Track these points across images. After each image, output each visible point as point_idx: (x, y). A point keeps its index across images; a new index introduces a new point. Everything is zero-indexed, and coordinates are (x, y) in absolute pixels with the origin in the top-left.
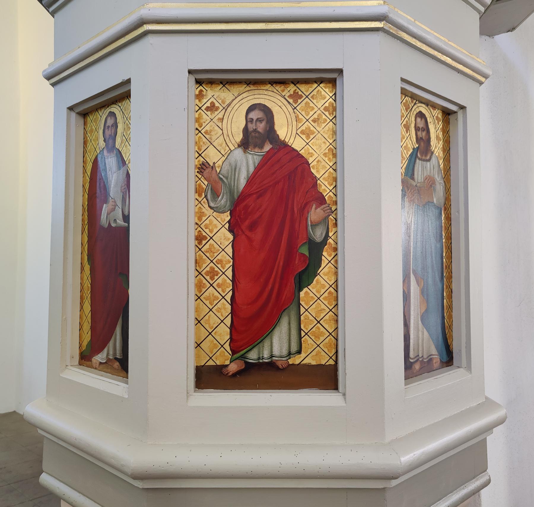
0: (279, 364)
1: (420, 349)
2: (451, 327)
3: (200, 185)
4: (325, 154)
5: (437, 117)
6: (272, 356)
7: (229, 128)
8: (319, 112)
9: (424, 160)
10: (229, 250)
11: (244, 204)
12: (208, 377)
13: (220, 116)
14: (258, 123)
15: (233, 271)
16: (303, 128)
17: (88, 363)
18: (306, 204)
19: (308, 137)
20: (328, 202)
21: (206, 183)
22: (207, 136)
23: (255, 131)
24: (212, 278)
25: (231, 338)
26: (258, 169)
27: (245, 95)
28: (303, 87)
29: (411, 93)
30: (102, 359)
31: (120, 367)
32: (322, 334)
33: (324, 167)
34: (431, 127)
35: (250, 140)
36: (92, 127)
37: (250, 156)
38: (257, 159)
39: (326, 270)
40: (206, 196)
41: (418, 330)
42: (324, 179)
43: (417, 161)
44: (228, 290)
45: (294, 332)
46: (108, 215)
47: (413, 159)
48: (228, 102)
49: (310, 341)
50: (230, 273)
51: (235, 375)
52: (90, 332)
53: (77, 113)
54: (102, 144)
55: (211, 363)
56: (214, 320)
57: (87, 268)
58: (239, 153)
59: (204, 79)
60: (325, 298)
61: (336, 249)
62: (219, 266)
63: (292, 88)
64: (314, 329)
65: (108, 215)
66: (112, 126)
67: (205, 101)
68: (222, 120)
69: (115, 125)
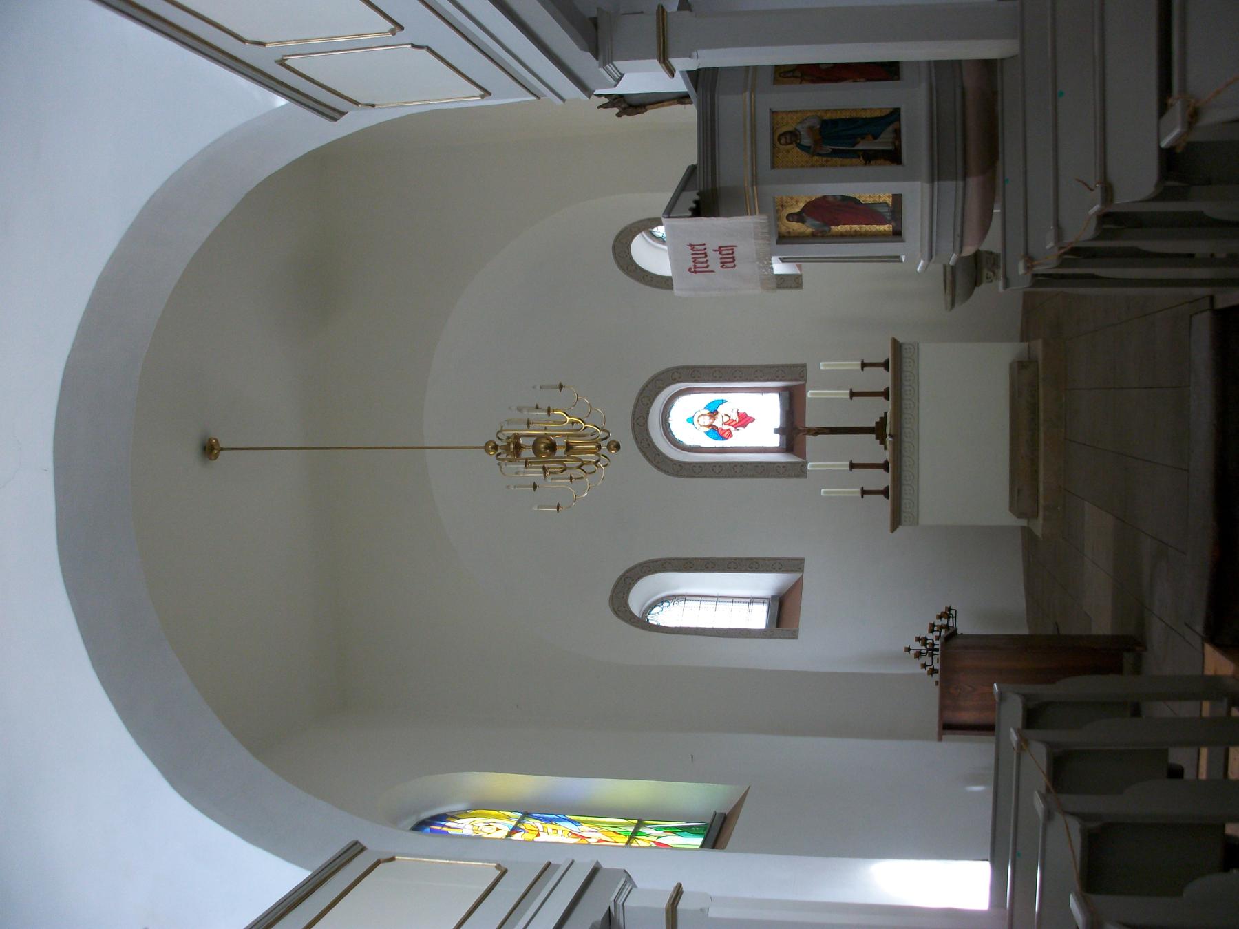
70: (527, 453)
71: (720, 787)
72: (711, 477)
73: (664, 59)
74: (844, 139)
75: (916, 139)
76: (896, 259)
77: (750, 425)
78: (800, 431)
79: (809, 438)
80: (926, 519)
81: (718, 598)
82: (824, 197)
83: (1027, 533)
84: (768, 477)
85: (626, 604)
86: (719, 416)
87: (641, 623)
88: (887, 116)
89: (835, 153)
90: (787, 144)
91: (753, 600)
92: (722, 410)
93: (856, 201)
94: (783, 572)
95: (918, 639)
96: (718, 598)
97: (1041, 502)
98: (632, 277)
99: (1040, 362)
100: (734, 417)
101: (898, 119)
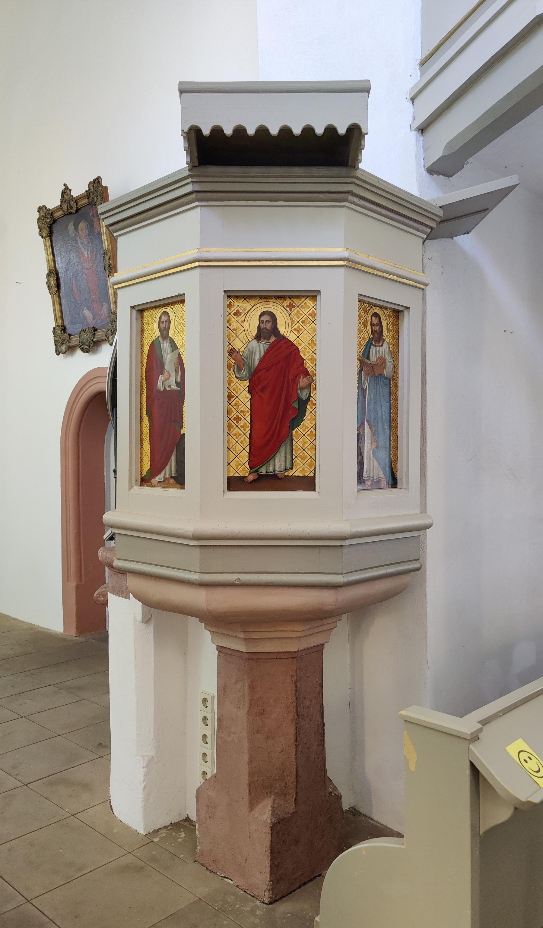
0: (279, 476)
1: (371, 472)
2: (396, 461)
3: (229, 363)
4: (309, 344)
5: (389, 315)
6: (275, 471)
7: (248, 327)
8: (306, 316)
9: (377, 346)
10: (248, 404)
11: (258, 375)
12: (234, 484)
13: (243, 319)
14: (267, 324)
15: (251, 418)
16: (295, 327)
17: (148, 484)
18: (297, 376)
19: (298, 333)
20: (311, 374)
21: (234, 362)
22: (234, 332)
23: (265, 328)
24: (237, 422)
25: (249, 459)
26: (266, 353)
27: (258, 305)
28: (296, 301)
29: (366, 303)
30: (160, 479)
31: (175, 482)
32: (306, 457)
33: (308, 352)
34: (384, 323)
35: (262, 334)
36: (148, 320)
37: (262, 345)
38: (266, 347)
39: (309, 417)
40: (233, 370)
41: (370, 460)
42: (308, 359)
43: (372, 346)
44: (247, 429)
45: (289, 456)
46: (166, 382)
47: (369, 345)
48: (247, 310)
49: (298, 461)
50: (248, 419)
51: (251, 482)
52: (149, 463)
53: (137, 310)
54: (158, 333)
55: (237, 475)
56: (239, 448)
57: (146, 419)
58: (255, 342)
59: (232, 295)
60: (308, 435)
61: (315, 404)
62: (242, 414)
63: (288, 301)
64: (301, 454)
65: (166, 382)
66: (166, 321)
67: (233, 309)
68: (244, 321)
69: (169, 321)
93: (298, 418)
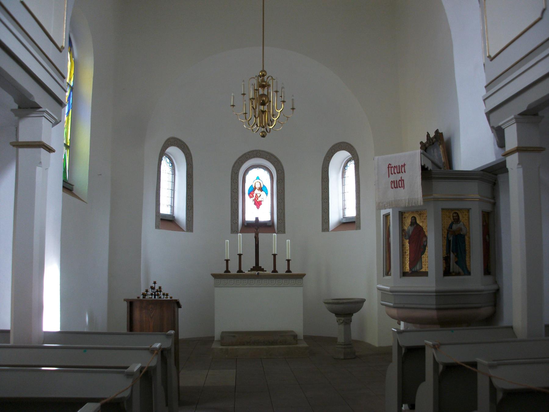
70: (261, 91)
71: (87, 188)
72: (231, 188)
73: (518, 150)
74: (455, 246)
75: (455, 283)
76: (387, 272)
77: (255, 206)
78: (257, 230)
79: (253, 235)
80: (217, 290)
81: (173, 190)
82: (426, 236)
83: (211, 340)
84: (231, 215)
85: (172, 145)
86: (259, 192)
87: (162, 153)
88: (466, 268)
89: (449, 242)
90: (453, 217)
91: (172, 207)
92: (263, 193)
93: (423, 252)
94: (187, 224)
95: (160, 288)
96: (173, 190)
97: (230, 347)
98: (328, 151)
99: (298, 345)
100: (260, 199)
101: (465, 275)
